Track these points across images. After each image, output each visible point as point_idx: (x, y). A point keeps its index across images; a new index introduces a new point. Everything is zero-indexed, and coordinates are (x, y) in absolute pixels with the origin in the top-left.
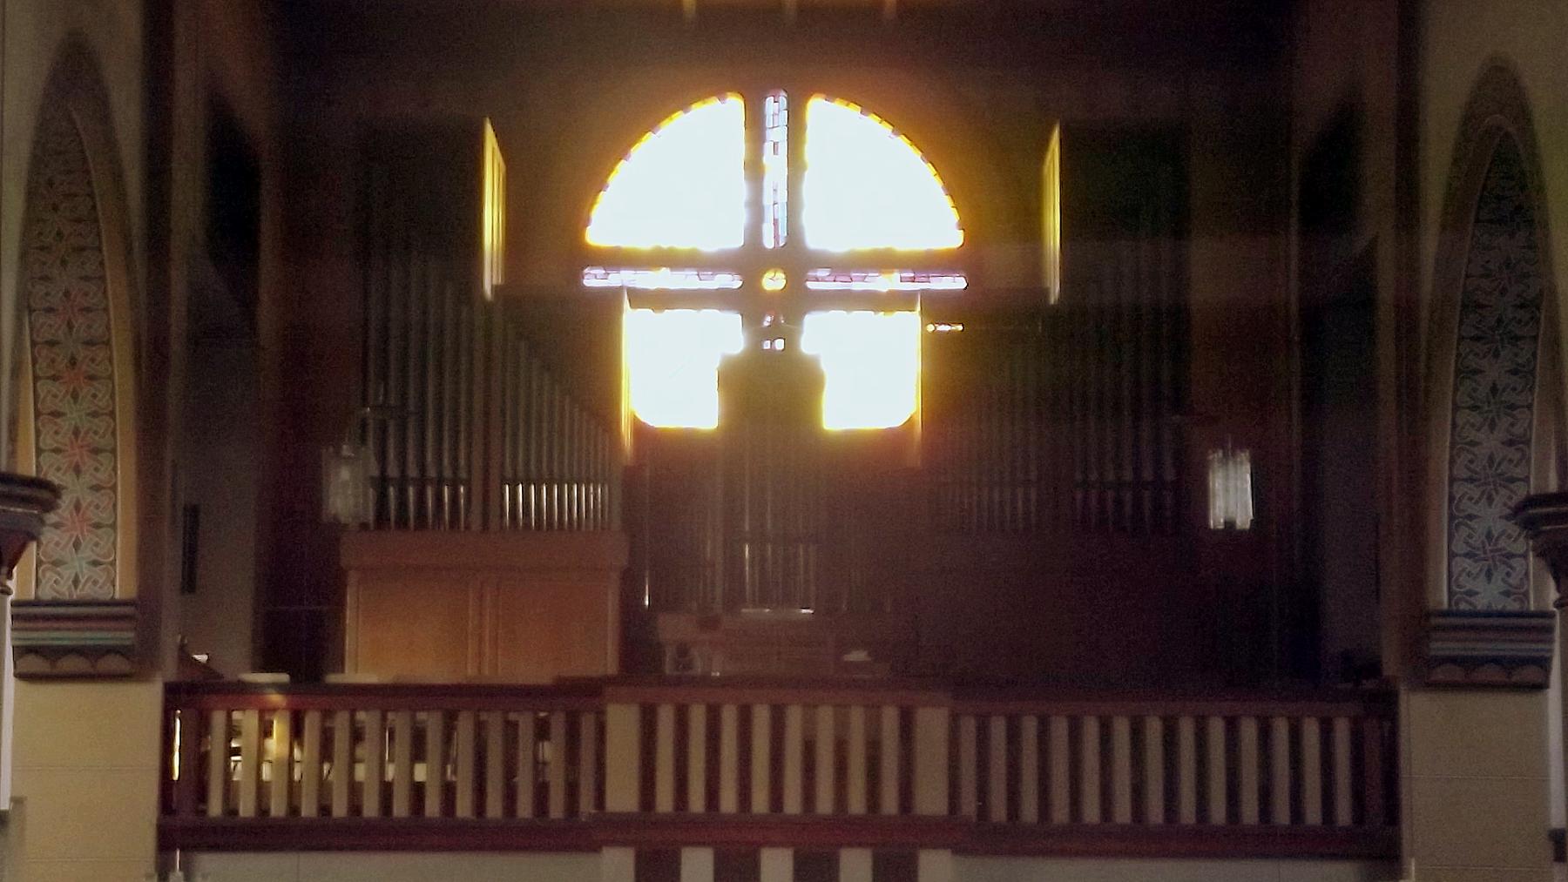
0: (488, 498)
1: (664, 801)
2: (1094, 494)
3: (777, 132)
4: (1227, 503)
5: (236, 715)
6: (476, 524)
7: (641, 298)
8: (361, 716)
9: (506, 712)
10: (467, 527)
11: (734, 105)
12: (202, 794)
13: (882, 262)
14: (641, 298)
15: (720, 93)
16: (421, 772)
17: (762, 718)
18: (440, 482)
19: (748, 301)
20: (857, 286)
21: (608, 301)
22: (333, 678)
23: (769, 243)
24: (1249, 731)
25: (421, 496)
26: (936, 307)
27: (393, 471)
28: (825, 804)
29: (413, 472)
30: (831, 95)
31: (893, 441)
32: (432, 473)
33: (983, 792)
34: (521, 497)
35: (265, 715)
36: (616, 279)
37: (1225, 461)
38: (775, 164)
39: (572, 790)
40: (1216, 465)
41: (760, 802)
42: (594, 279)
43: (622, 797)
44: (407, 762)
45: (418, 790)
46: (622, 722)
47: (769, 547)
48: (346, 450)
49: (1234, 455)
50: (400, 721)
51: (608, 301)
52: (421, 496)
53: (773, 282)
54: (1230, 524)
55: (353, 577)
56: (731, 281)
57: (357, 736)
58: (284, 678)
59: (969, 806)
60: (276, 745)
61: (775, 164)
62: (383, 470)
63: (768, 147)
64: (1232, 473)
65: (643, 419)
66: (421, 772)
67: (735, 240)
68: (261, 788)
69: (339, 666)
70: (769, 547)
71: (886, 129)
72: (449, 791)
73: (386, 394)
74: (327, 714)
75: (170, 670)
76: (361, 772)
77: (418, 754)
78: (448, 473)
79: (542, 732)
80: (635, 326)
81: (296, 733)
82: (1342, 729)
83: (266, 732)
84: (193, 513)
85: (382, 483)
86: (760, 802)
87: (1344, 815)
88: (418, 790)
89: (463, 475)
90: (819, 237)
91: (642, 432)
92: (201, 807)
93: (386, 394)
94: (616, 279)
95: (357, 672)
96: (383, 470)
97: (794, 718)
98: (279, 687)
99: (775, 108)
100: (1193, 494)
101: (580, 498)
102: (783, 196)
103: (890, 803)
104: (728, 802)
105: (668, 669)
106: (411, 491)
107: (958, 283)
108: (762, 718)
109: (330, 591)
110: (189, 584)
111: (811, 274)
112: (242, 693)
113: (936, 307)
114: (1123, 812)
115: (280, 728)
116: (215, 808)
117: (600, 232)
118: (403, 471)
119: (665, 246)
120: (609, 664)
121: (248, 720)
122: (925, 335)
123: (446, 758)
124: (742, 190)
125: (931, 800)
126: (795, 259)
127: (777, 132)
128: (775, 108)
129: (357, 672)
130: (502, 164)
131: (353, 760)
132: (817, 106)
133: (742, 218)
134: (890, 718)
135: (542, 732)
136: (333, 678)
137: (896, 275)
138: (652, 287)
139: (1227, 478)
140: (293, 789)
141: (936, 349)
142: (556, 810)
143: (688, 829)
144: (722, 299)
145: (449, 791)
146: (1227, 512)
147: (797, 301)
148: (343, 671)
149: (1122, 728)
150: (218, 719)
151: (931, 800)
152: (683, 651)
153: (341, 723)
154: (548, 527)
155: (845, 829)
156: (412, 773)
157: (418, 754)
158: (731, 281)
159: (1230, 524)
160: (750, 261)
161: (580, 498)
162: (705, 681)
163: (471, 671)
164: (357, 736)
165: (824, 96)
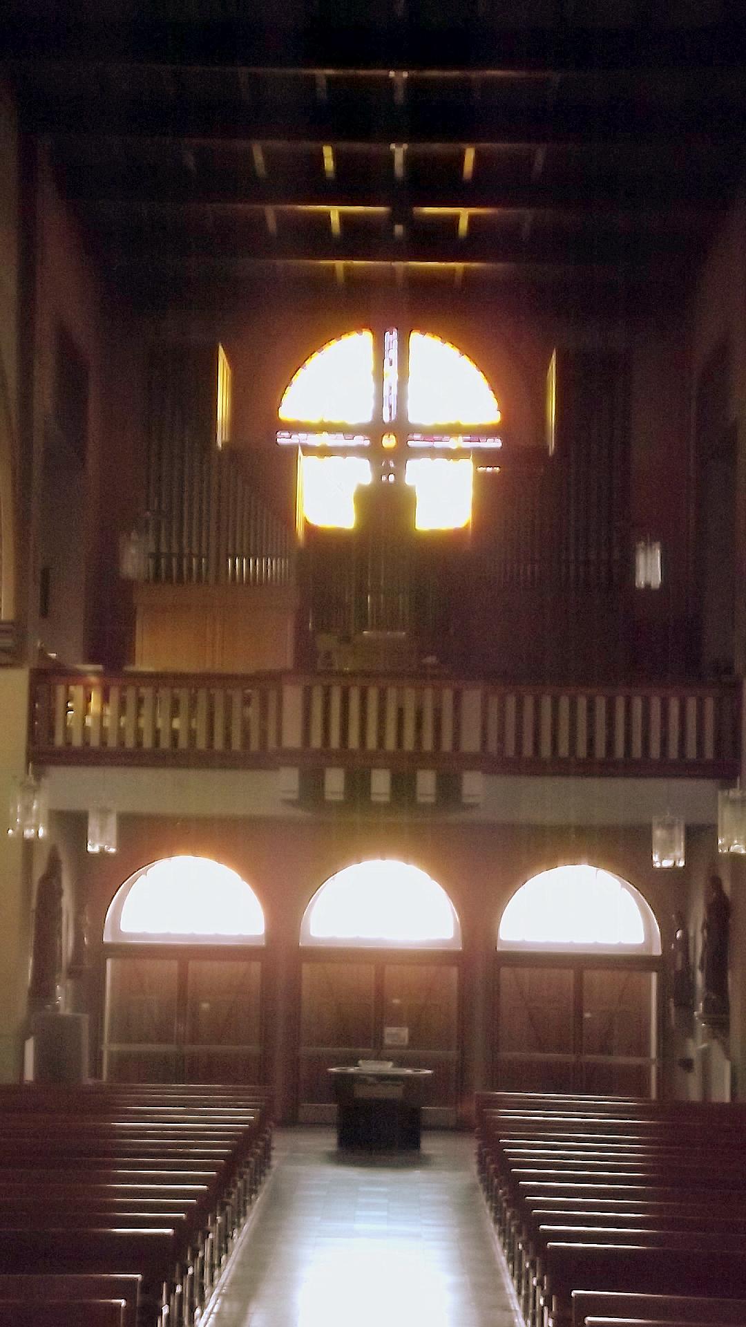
0: (220, 564)
1: (316, 742)
2: (572, 567)
3: (392, 353)
4: (646, 573)
5: (72, 688)
6: (212, 581)
7: (308, 450)
8: (143, 690)
9: (244, 690)
10: (207, 581)
11: (367, 337)
12: (52, 732)
13: (454, 430)
14: (308, 450)
15: (359, 328)
16: (176, 724)
17: (373, 694)
18: (191, 554)
19: (375, 453)
20: (438, 445)
21: (291, 452)
22: (129, 668)
23: (386, 419)
24: (564, 704)
25: (180, 566)
26: (484, 457)
27: (164, 549)
28: (409, 745)
29: (175, 550)
30: (423, 330)
31: (455, 537)
32: (186, 551)
33: (501, 739)
34: (240, 566)
35: (87, 688)
36: (298, 439)
37: (645, 549)
38: (391, 373)
39: (264, 734)
40: (641, 550)
41: (372, 742)
42: (283, 439)
43: (292, 739)
44: (169, 719)
45: (174, 735)
46: (292, 697)
47: (382, 596)
48: (134, 536)
49: (651, 545)
50: (164, 693)
51: (291, 452)
52: (180, 566)
53: (389, 442)
54: (648, 586)
55: (140, 610)
56: (361, 441)
57: (140, 701)
58: (100, 667)
59: (493, 746)
60: (95, 705)
61: (391, 373)
62: (158, 549)
63: (387, 362)
64: (649, 555)
65: (308, 519)
66: (176, 724)
67: (366, 417)
68: (85, 729)
69: (133, 662)
70: (382, 596)
71: (456, 351)
72: (192, 735)
73: (160, 503)
74: (123, 689)
75: (33, 662)
76: (143, 722)
77: (174, 713)
78: (195, 551)
79: (247, 702)
80: (307, 468)
81: (105, 699)
82: (710, 704)
83: (88, 699)
84: (45, 573)
85: (156, 556)
86: (372, 742)
87: (709, 754)
88: (174, 735)
89: (204, 551)
90: (415, 417)
91: (310, 530)
92: (51, 740)
93: (160, 503)
94: (298, 439)
95: (144, 664)
96: (158, 549)
97: (392, 694)
98: (96, 673)
99: (391, 338)
100: (629, 568)
101: (273, 567)
102: (395, 391)
103: (447, 745)
104: (354, 742)
105: (320, 667)
106: (174, 560)
107: (495, 443)
108: (373, 694)
109: (128, 621)
110: (44, 613)
111: (410, 437)
112: (76, 677)
113: (484, 457)
114: (673, 753)
115: (95, 698)
116: (59, 740)
117: (286, 412)
118: (200, 552)
119: (326, 420)
120: (288, 661)
121: (77, 691)
122: (476, 472)
123: (138, 715)
124: (371, 386)
125: (471, 743)
126: (402, 428)
127: (392, 353)
128: (391, 338)
129: (144, 664)
130: (229, 371)
131: (138, 715)
132: (415, 337)
133: (371, 405)
134: (448, 695)
135: (247, 702)
136: (129, 668)
137: (461, 438)
138: (318, 445)
139: (646, 557)
140: (103, 731)
141: (485, 486)
142: (254, 745)
143: (419, 759)
144: (359, 451)
145: (192, 735)
146: (646, 578)
147: (403, 454)
148: (134, 664)
149: (601, 704)
150: (61, 691)
151: (471, 743)
152: (328, 655)
153: (130, 694)
154: (253, 583)
155: (419, 759)
156: (171, 725)
157: (174, 713)
158: (361, 441)
159: (648, 586)
160: (376, 430)
161: (273, 567)
162: (341, 674)
163: (208, 666)
164: (140, 701)
165: (419, 331)
